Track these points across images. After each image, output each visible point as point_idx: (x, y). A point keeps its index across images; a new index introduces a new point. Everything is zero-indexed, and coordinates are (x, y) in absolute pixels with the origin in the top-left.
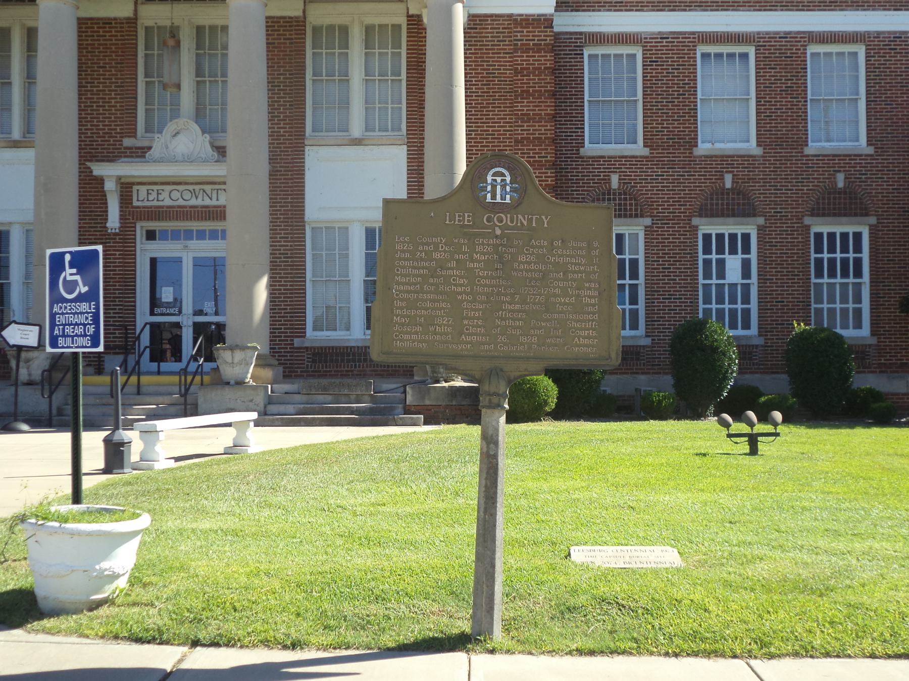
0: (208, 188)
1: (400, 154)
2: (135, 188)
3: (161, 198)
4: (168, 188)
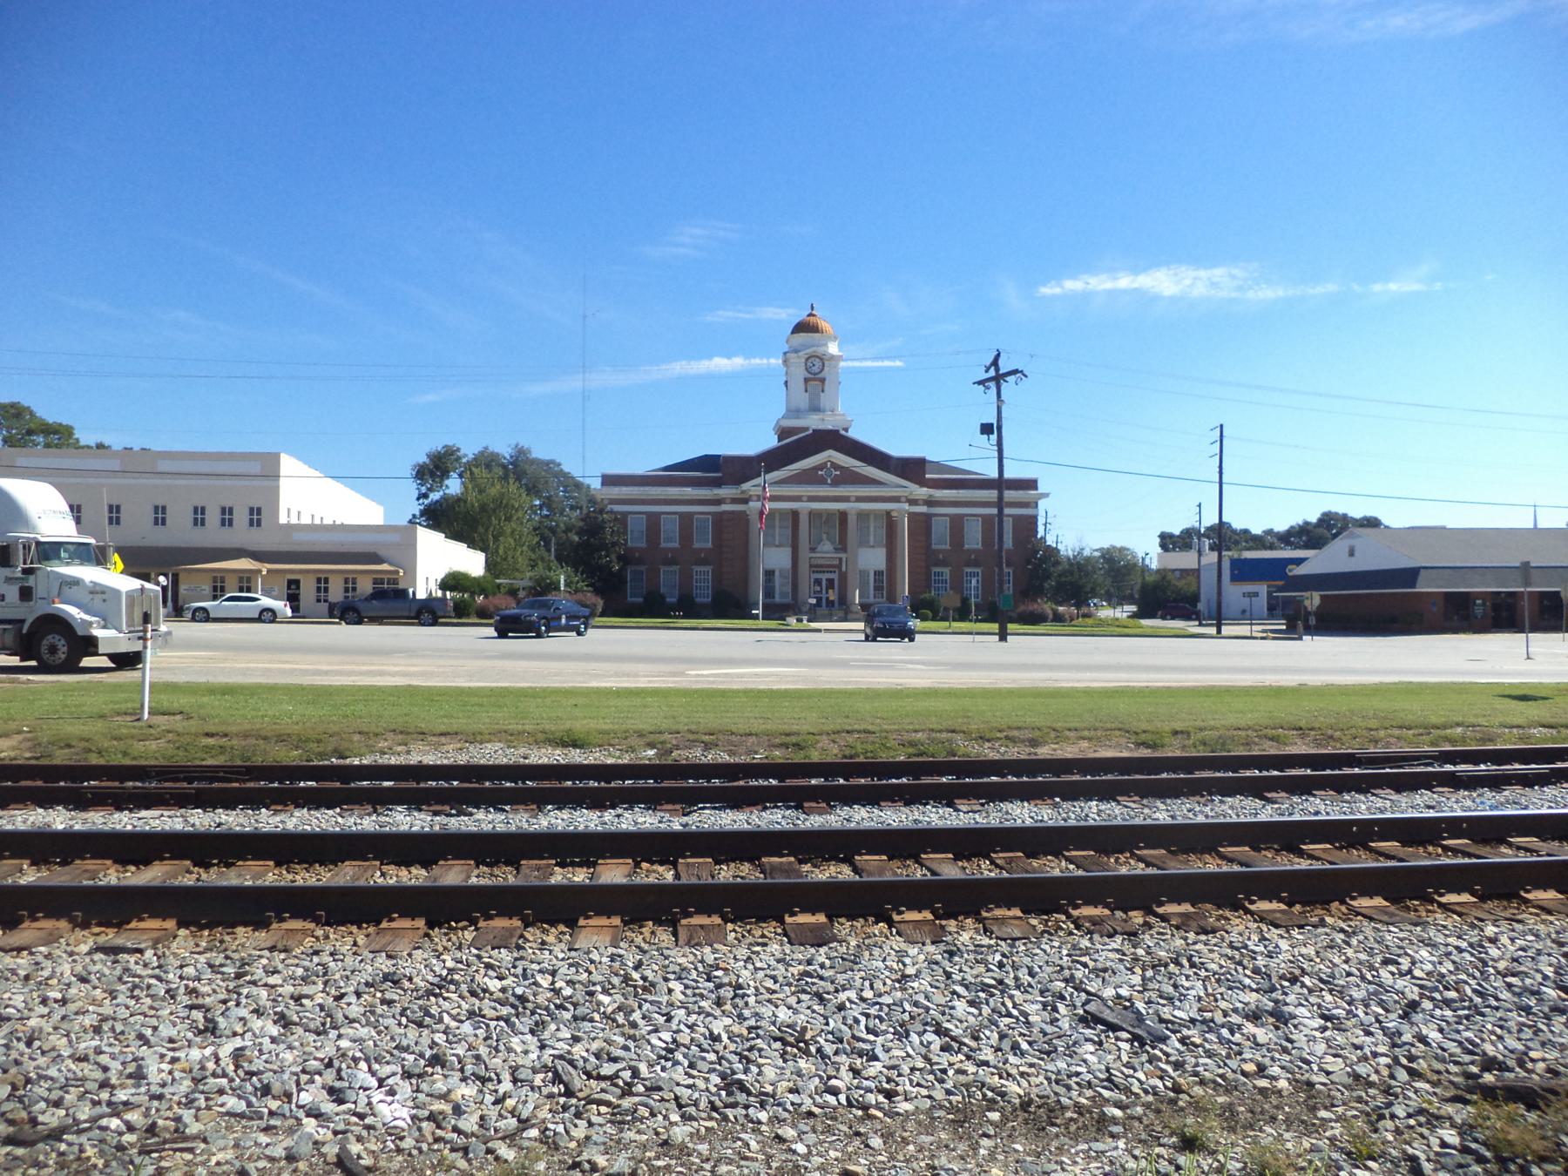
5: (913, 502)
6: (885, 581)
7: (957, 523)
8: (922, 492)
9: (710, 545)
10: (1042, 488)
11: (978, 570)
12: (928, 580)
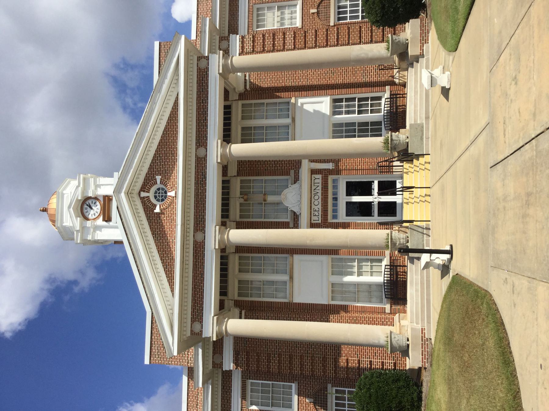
0: (313, 188)
1: (296, 257)
2: (313, 222)
3: (317, 210)
4: (313, 206)
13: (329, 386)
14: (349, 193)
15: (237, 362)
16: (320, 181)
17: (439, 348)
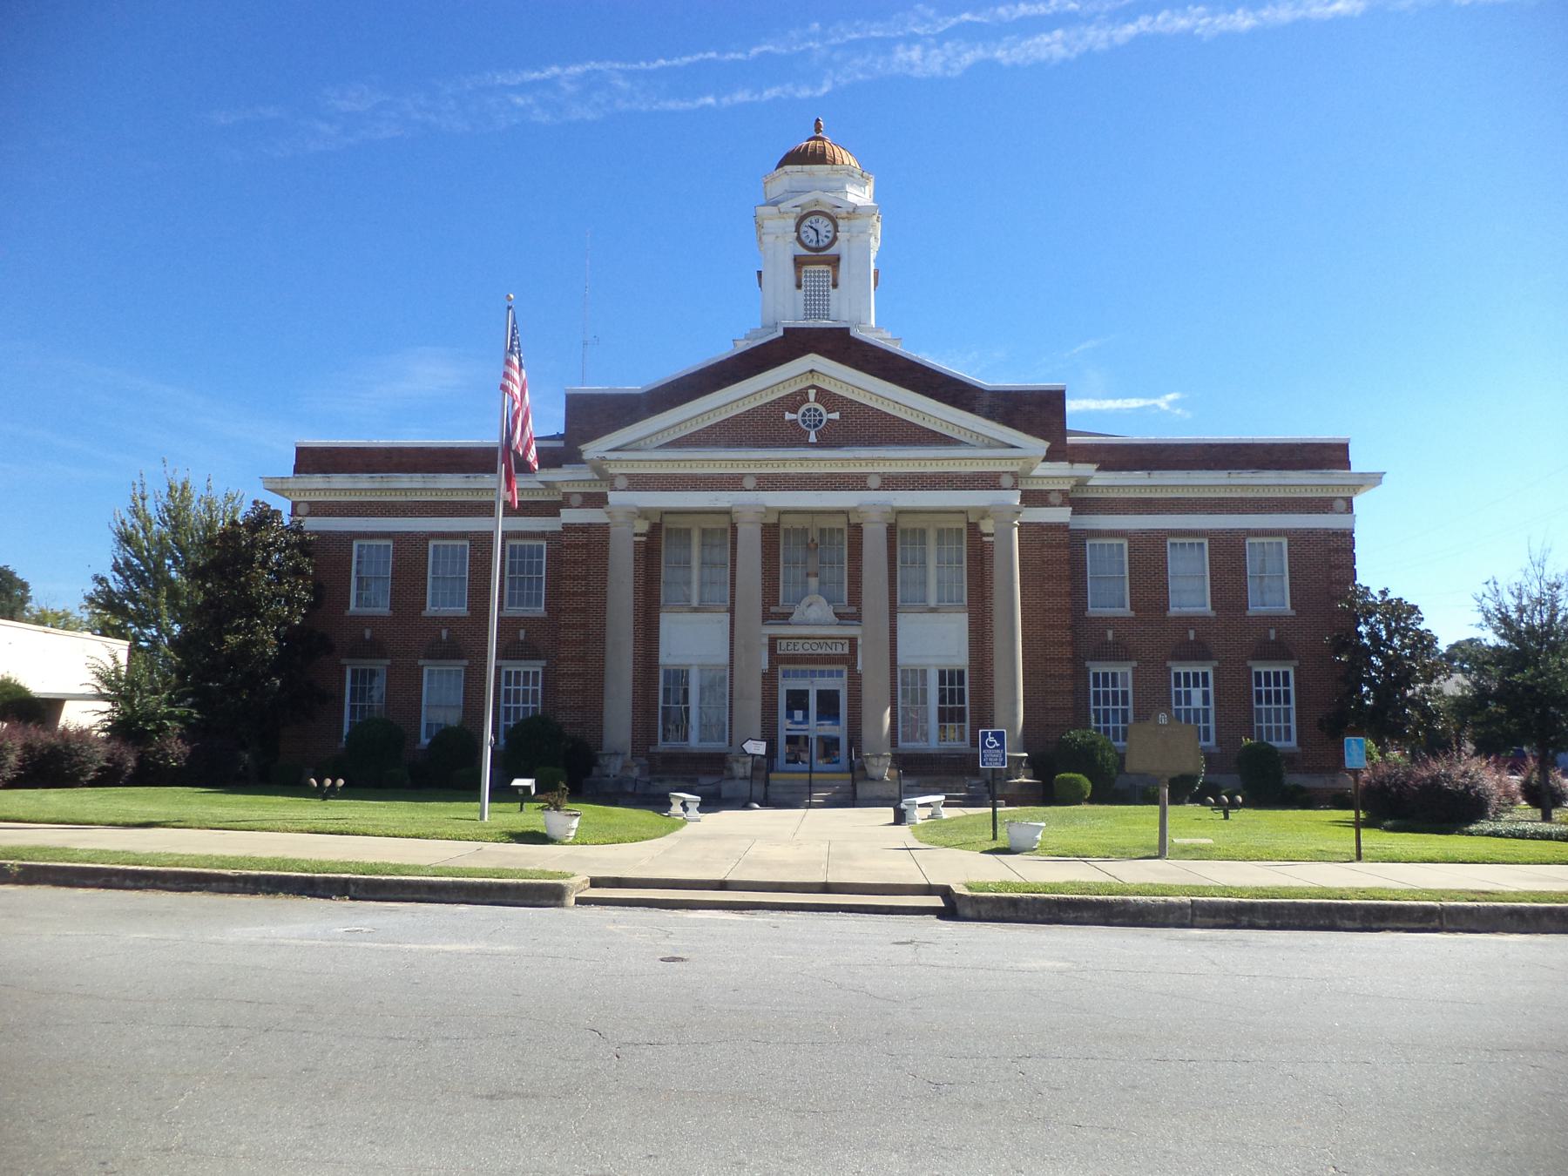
1: (726, 617)
5: (1033, 498)
6: (967, 696)
7: (1148, 555)
8: (1059, 474)
9: (540, 611)
10: (1360, 462)
11: (1208, 668)
12: (1080, 694)
13: (543, 663)
14: (821, 694)
15: (568, 528)
16: (839, 651)
17: (39, 736)
